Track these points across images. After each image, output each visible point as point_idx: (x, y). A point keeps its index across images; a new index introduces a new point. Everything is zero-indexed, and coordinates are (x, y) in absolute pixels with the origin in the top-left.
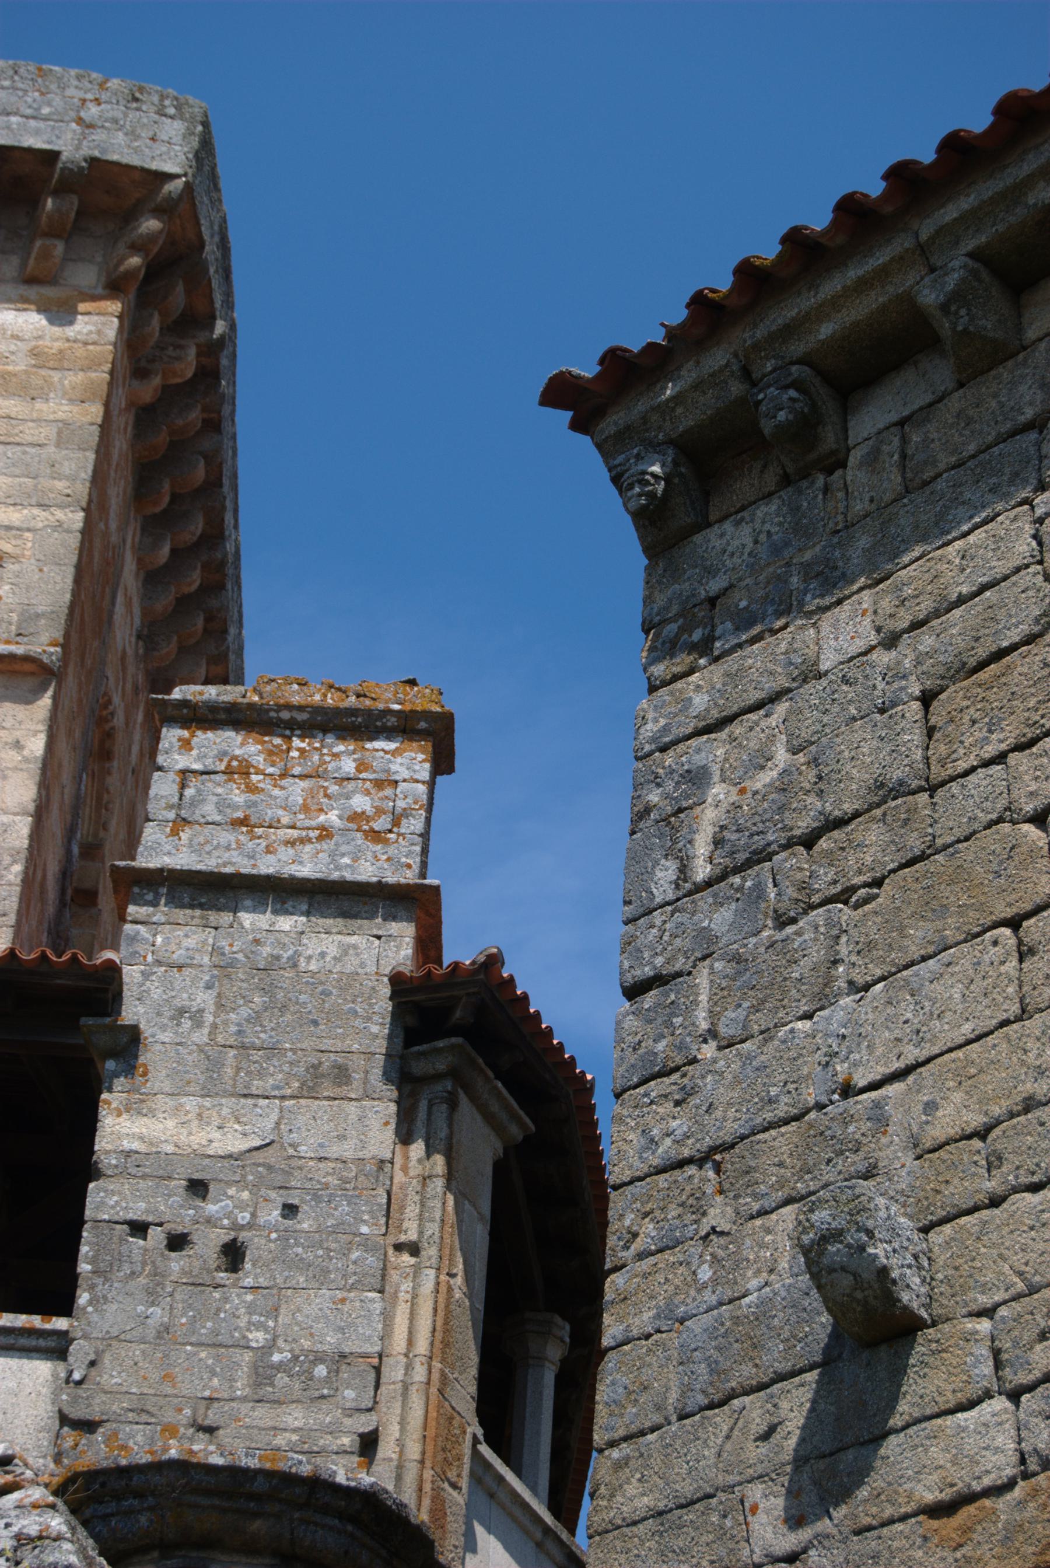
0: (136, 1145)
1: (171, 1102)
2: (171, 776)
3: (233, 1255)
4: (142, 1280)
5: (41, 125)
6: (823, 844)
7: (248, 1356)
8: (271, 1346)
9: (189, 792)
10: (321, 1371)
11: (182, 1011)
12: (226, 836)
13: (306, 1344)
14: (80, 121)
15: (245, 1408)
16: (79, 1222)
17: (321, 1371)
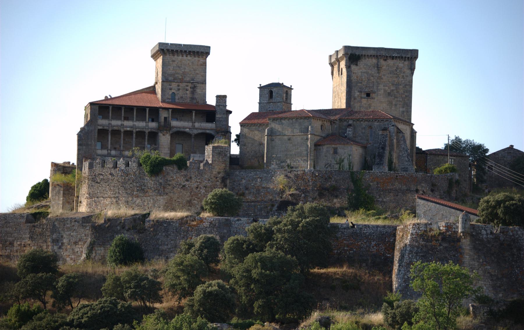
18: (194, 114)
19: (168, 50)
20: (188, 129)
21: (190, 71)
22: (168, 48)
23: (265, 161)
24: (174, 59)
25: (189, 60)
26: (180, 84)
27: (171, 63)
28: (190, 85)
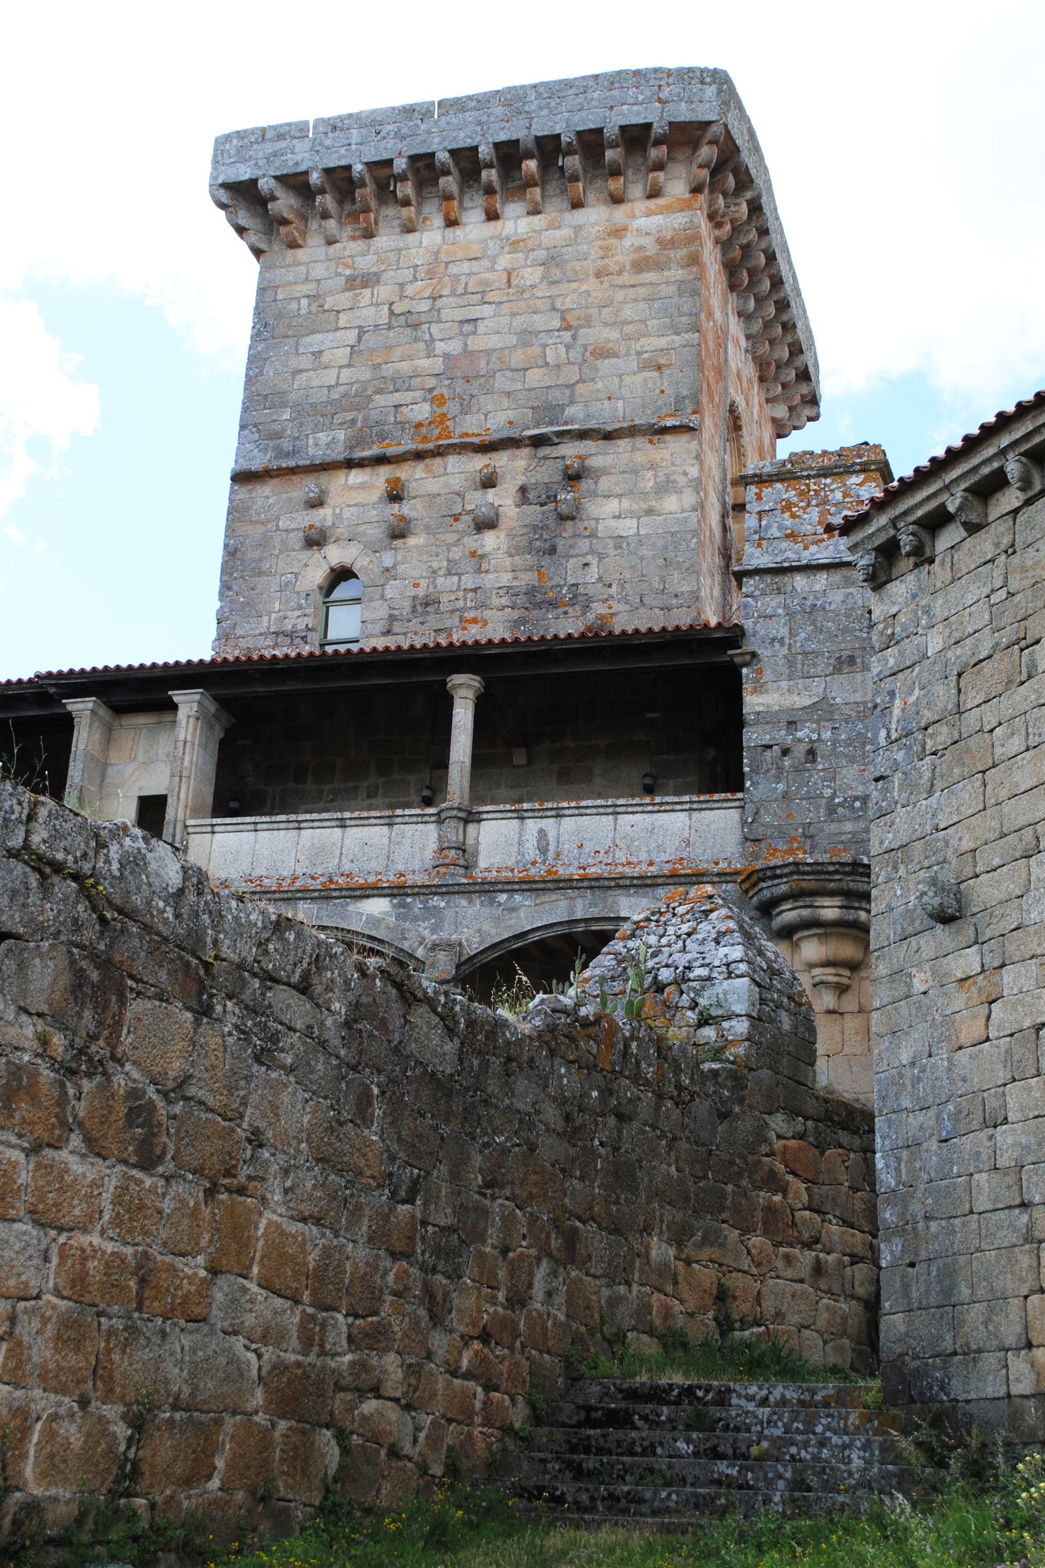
0: (761, 709)
1: (775, 685)
2: (754, 515)
3: (811, 753)
4: (773, 772)
5: (640, 108)
6: (930, 731)
7: (824, 801)
8: (834, 795)
9: (764, 523)
10: (857, 804)
11: (773, 639)
12: (784, 545)
13: (850, 792)
14: (659, 100)
15: (825, 826)
16: (741, 749)
17: (857, 804)
18: (463, 717)
19: (296, 183)
20: (378, 906)
21: (526, 336)
22: (301, 158)
23: (649, 715)
24: (366, 263)
25: (515, 244)
26: (413, 474)
27: (344, 300)
28: (515, 467)
